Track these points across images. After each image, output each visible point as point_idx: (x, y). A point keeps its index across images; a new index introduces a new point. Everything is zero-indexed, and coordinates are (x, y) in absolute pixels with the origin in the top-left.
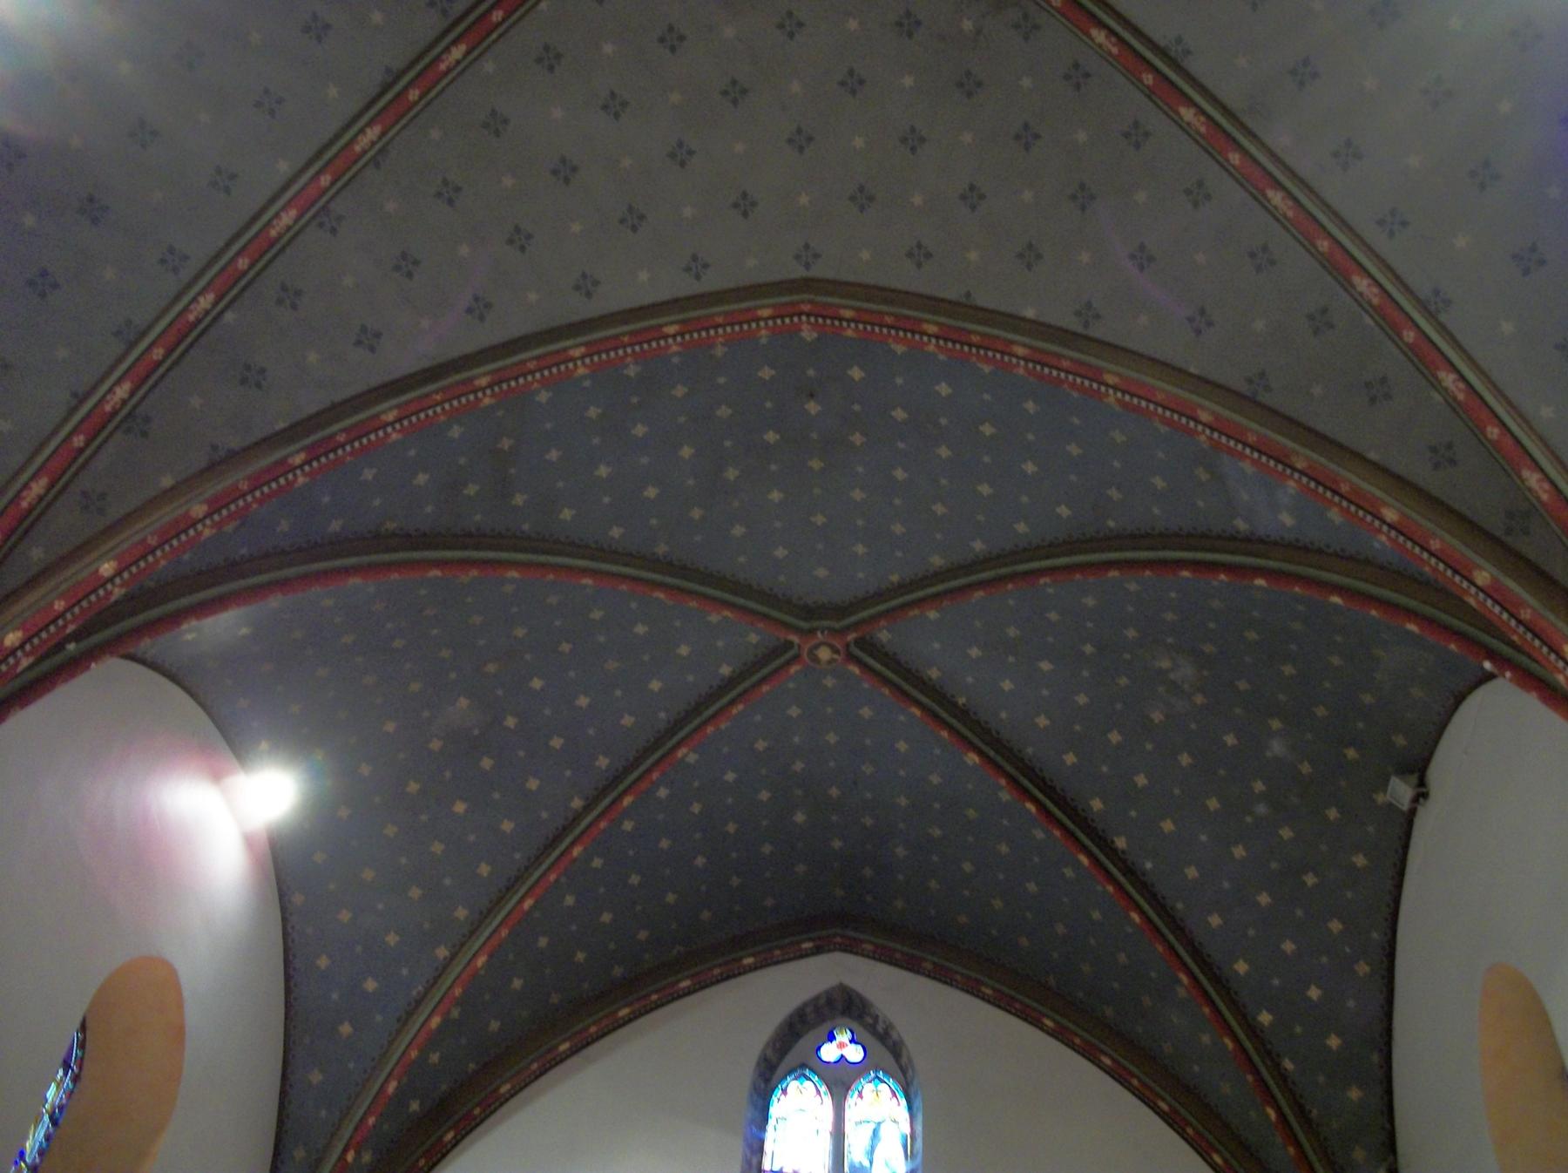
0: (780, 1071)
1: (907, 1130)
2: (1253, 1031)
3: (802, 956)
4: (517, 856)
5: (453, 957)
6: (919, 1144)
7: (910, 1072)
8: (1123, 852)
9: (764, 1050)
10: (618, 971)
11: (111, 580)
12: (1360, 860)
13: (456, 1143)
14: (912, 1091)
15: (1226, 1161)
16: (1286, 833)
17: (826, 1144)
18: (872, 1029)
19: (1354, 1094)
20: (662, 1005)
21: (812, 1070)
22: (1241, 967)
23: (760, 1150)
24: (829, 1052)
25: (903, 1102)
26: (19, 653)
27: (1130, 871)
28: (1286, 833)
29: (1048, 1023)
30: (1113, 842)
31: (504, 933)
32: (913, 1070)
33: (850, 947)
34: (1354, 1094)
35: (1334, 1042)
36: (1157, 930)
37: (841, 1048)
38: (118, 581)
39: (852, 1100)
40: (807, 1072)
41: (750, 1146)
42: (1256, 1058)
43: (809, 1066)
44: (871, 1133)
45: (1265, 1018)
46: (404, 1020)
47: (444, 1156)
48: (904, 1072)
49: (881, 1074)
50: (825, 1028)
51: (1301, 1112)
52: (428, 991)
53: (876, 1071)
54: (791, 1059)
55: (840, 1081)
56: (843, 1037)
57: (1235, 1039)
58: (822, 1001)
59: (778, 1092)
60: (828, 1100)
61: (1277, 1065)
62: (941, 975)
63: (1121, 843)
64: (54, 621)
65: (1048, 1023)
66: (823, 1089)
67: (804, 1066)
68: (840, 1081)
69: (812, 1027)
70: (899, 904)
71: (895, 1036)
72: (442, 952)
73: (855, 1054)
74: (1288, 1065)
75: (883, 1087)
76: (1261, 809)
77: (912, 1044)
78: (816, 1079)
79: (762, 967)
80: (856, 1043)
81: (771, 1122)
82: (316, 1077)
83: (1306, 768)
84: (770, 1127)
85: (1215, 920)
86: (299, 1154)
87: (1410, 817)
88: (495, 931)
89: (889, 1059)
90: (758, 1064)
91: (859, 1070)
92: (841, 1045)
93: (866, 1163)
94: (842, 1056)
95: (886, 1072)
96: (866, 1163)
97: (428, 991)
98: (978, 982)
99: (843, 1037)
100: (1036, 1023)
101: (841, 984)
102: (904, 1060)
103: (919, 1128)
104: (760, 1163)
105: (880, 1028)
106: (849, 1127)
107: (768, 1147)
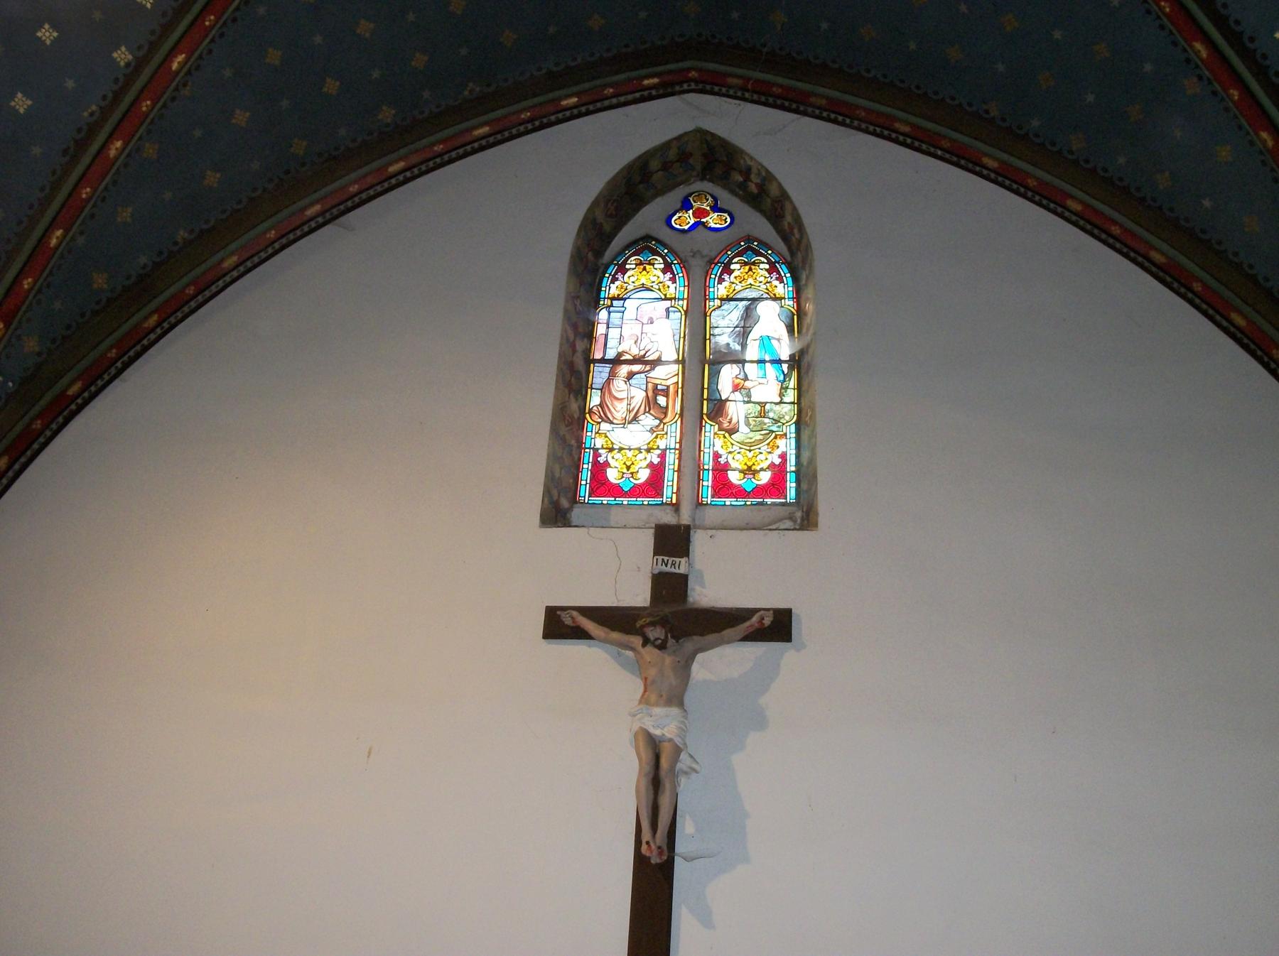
58: (672, 154)
69: (660, 192)
71: (774, 190)
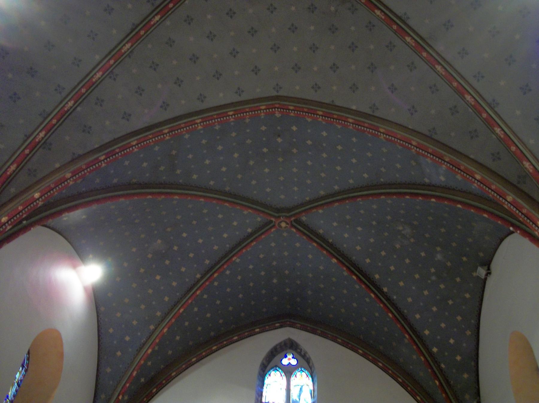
0: (268, 368)
1: (312, 388)
2: (431, 354)
3: (276, 329)
4: (178, 294)
5: (156, 329)
6: (316, 393)
7: (313, 368)
8: (386, 293)
9: (263, 361)
10: (212, 334)
11: (38, 199)
12: (467, 296)
13: (157, 393)
14: (314, 375)
15: (421, 399)
16: (442, 286)
17: (284, 393)
18: (300, 353)
19: (466, 376)
20: (228, 345)
21: (279, 368)
22: (427, 332)
23: (261, 395)
24: (285, 362)
25: (311, 379)
26: (7, 224)
27: (388, 299)
28: (442, 286)
29: (360, 351)
30: (382, 289)
31: (173, 320)
32: (314, 368)
33: (292, 325)
34: (466, 376)
35: (458, 358)
36: (398, 319)
37: (289, 360)
38: (40, 199)
39: (293, 378)
40: (277, 368)
41: (258, 394)
42: (432, 364)
43: (278, 366)
44: (299, 389)
45: (435, 350)
46: (139, 350)
47: (153, 397)
48: (311, 368)
49: (303, 369)
50: (284, 353)
51: (447, 382)
52: (147, 340)
53: (301, 368)
54: (272, 364)
55: (289, 372)
56: (290, 356)
57: (425, 357)
58: (283, 344)
59: (267, 375)
60: (285, 378)
61: (439, 366)
62: (324, 335)
63: (385, 290)
64: (19, 213)
65: (360, 351)
66: (283, 374)
67: (276, 366)
68: (289, 372)
69: (279, 353)
70: (309, 311)
71: (307, 356)
72: (152, 327)
73: (294, 362)
74: (443, 366)
75: (304, 373)
76: (434, 278)
77: (313, 359)
78: (280, 371)
79: (262, 332)
80: (294, 358)
81: (265, 386)
82: (109, 370)
83: (449, 264)
84: (265, 387)
85: (418, 316)
86: (103, 396)
87: (485, 281)
88: (170, 320)
89: (305, 364)
90: (261, 366)
91: (295, 368)
92: (289, 359)
93: (298, 400)
94: (290, 363)
95: (305, 368)
96: (298, 400)
97: (147, 340)
98: (336, 337)
99: (290, 356)
100: (356, 351)
101: (289, 338)
102: (311, 364)
103: (316, 388)
104: (261, 399)
105: (303, 353)
106: (292, 387)
107: (264, 394)
